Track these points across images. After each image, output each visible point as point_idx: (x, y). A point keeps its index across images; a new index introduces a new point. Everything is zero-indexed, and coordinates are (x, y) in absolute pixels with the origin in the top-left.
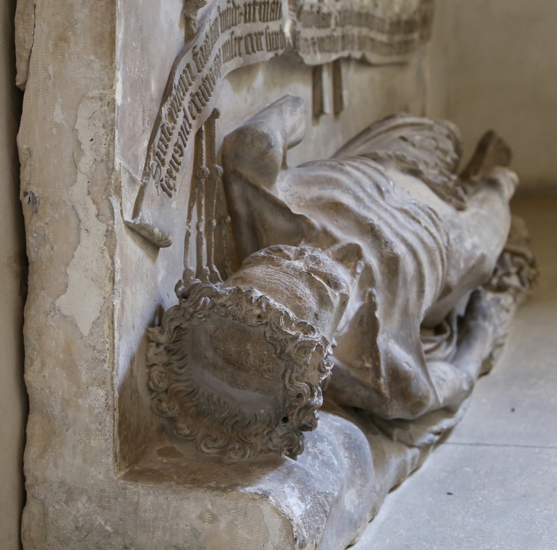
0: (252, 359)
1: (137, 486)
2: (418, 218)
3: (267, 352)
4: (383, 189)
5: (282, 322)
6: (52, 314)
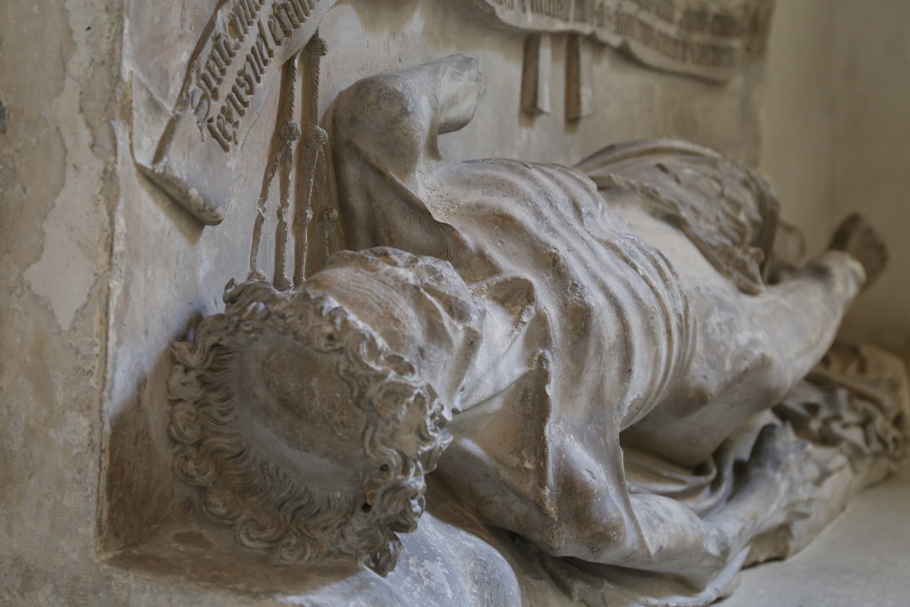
3: (341, 393)
5: (364, 350)
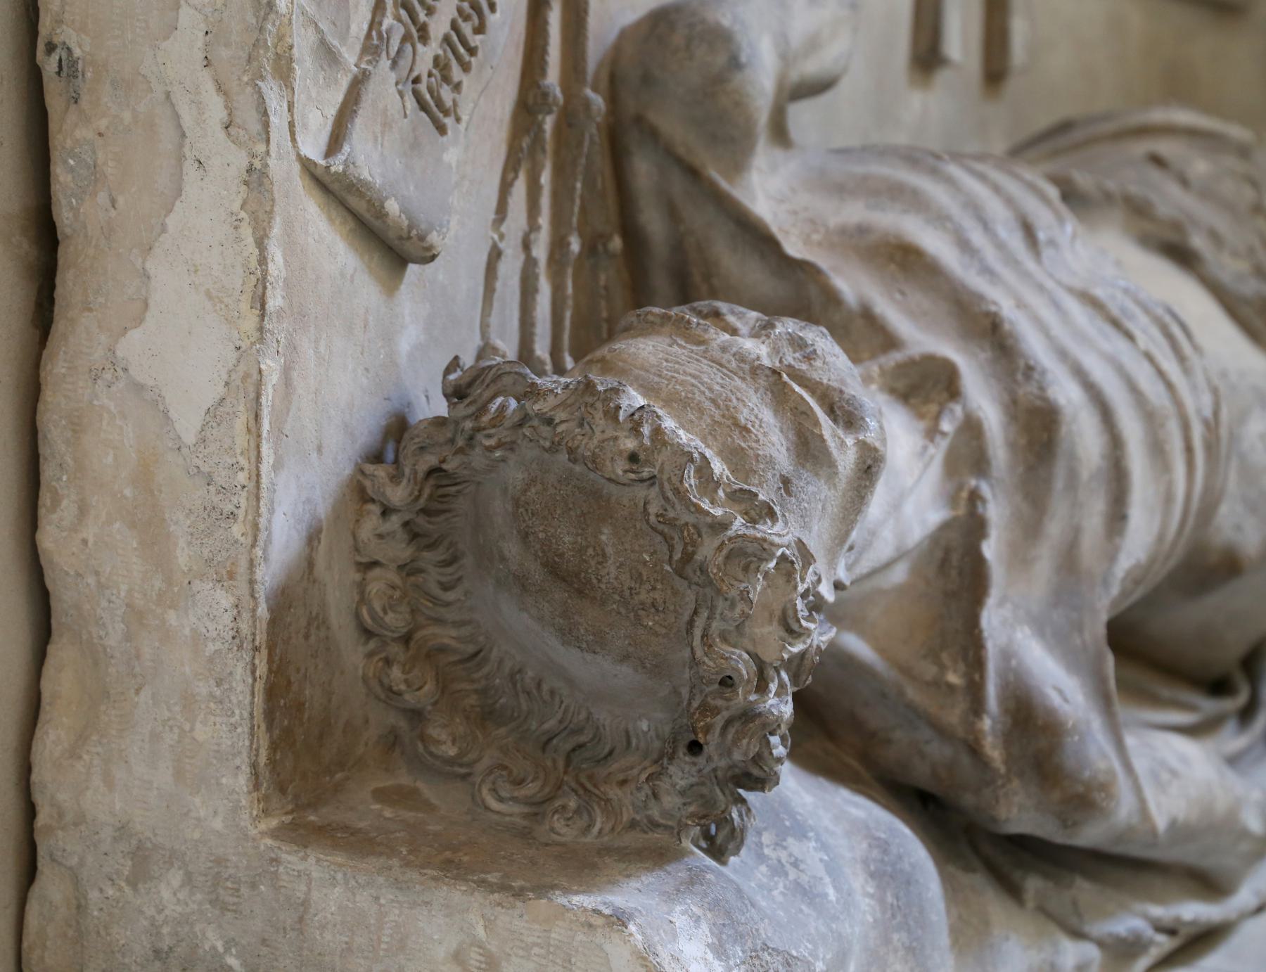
0: (613, 572)
1: (304, 858)
2: (1130, 325)
3: (652, 554)
4: (1042, 236)
5: (691, 480)
6: (108, 376)
